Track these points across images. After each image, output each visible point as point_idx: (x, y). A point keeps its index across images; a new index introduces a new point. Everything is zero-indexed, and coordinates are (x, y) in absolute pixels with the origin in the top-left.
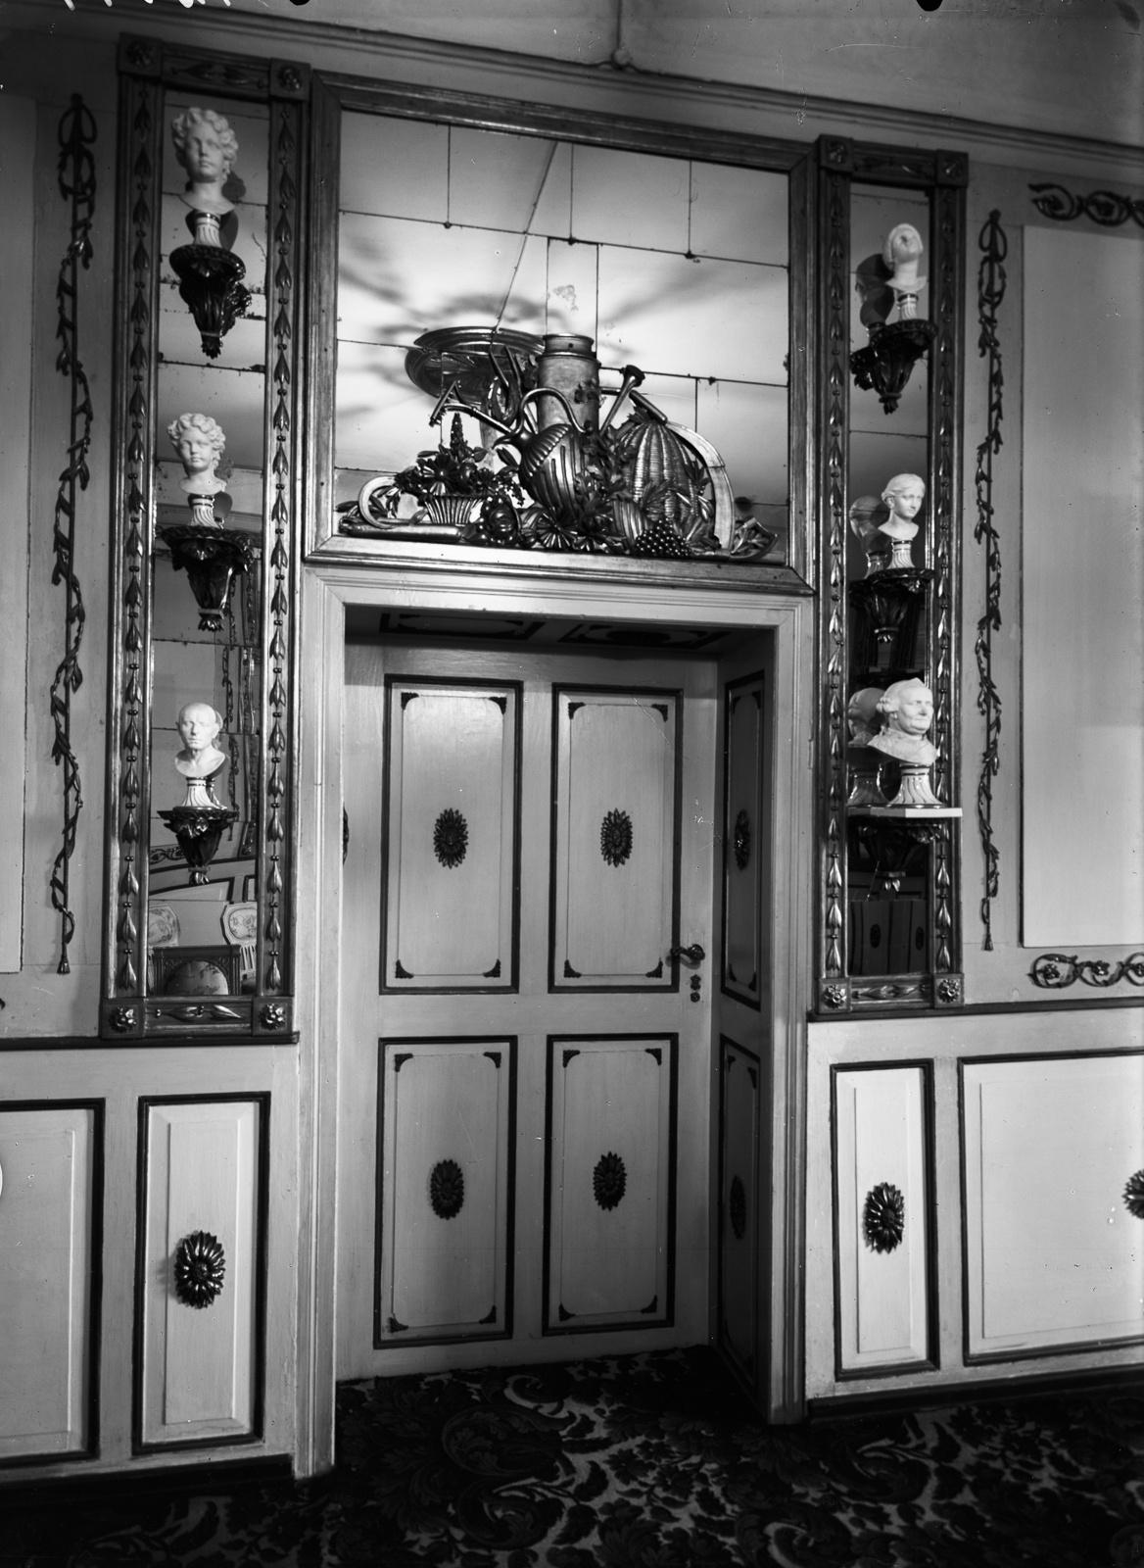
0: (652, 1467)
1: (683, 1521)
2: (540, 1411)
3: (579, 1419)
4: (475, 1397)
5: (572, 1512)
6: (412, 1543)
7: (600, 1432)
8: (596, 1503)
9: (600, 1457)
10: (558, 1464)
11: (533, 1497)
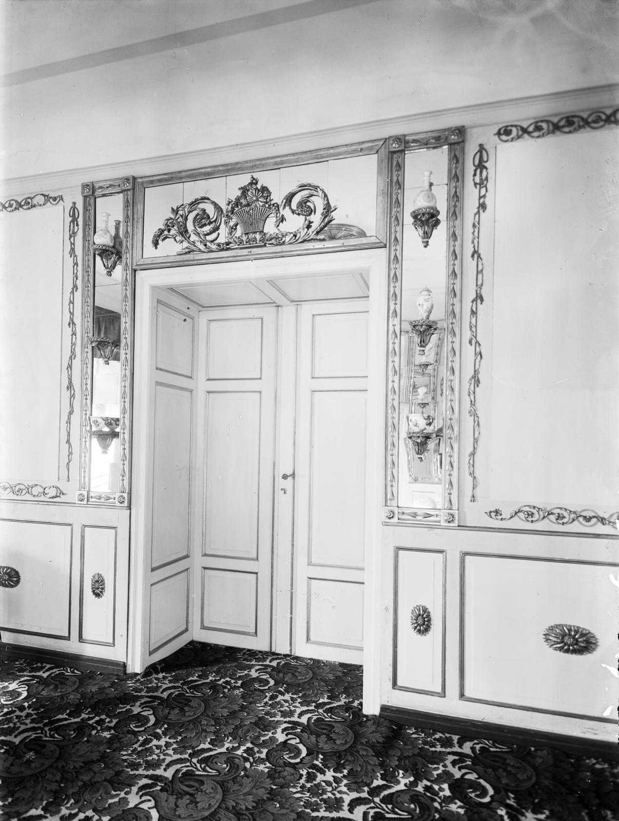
0: (435, 739)
1: (329, 775)
2: (477, 777)
3: (457, 767)
4: (512, 796)
5: (378, 796)
6: (460, 807)
7: (451, 758)
8: (365, 795)
9: (456, 749)
10: (478, 752)
11: (392, 808)
